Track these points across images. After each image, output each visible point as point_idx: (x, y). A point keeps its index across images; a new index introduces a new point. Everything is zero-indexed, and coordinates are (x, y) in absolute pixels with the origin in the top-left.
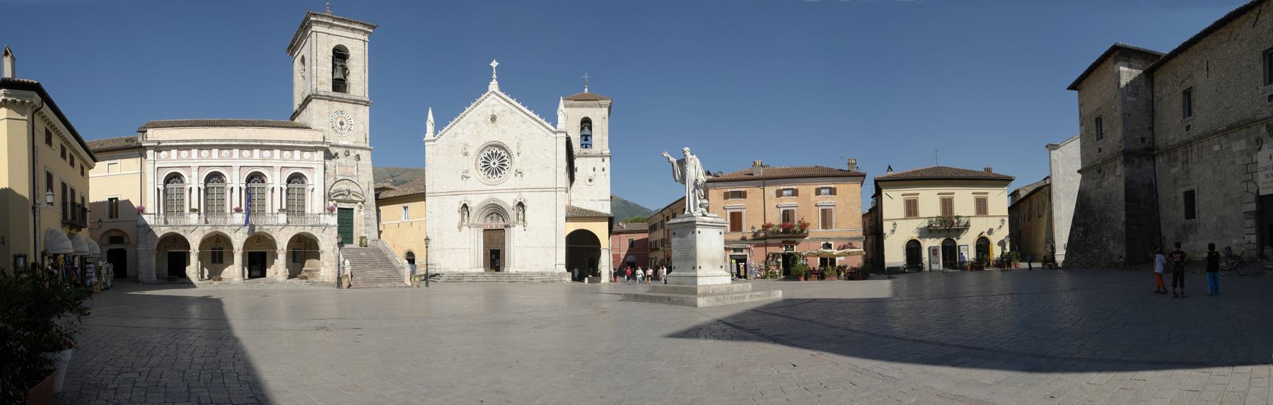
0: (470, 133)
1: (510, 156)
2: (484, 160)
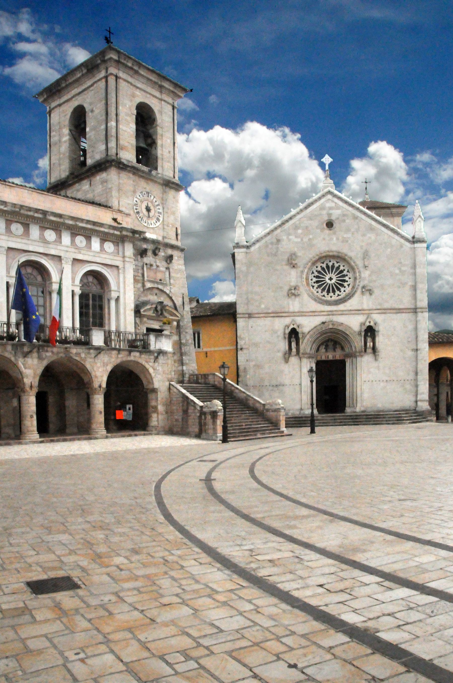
0: (299, 240)
1: (352, 269)
2: (316, 274)
